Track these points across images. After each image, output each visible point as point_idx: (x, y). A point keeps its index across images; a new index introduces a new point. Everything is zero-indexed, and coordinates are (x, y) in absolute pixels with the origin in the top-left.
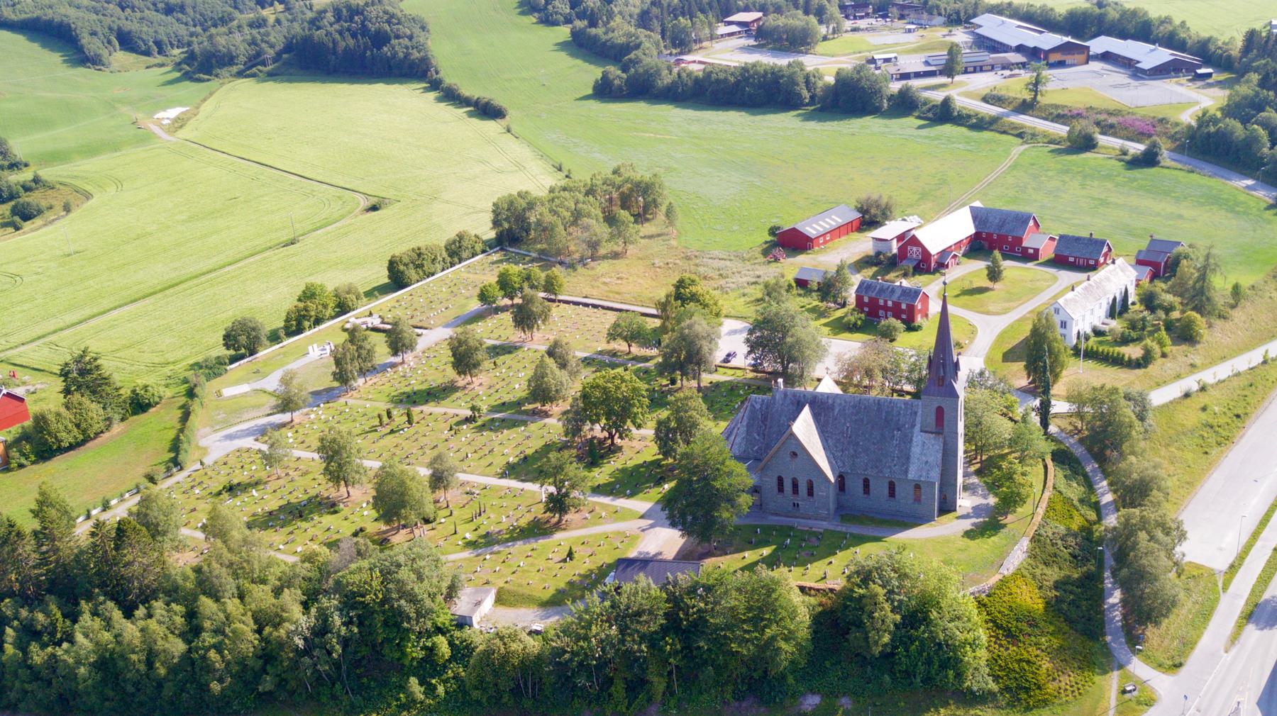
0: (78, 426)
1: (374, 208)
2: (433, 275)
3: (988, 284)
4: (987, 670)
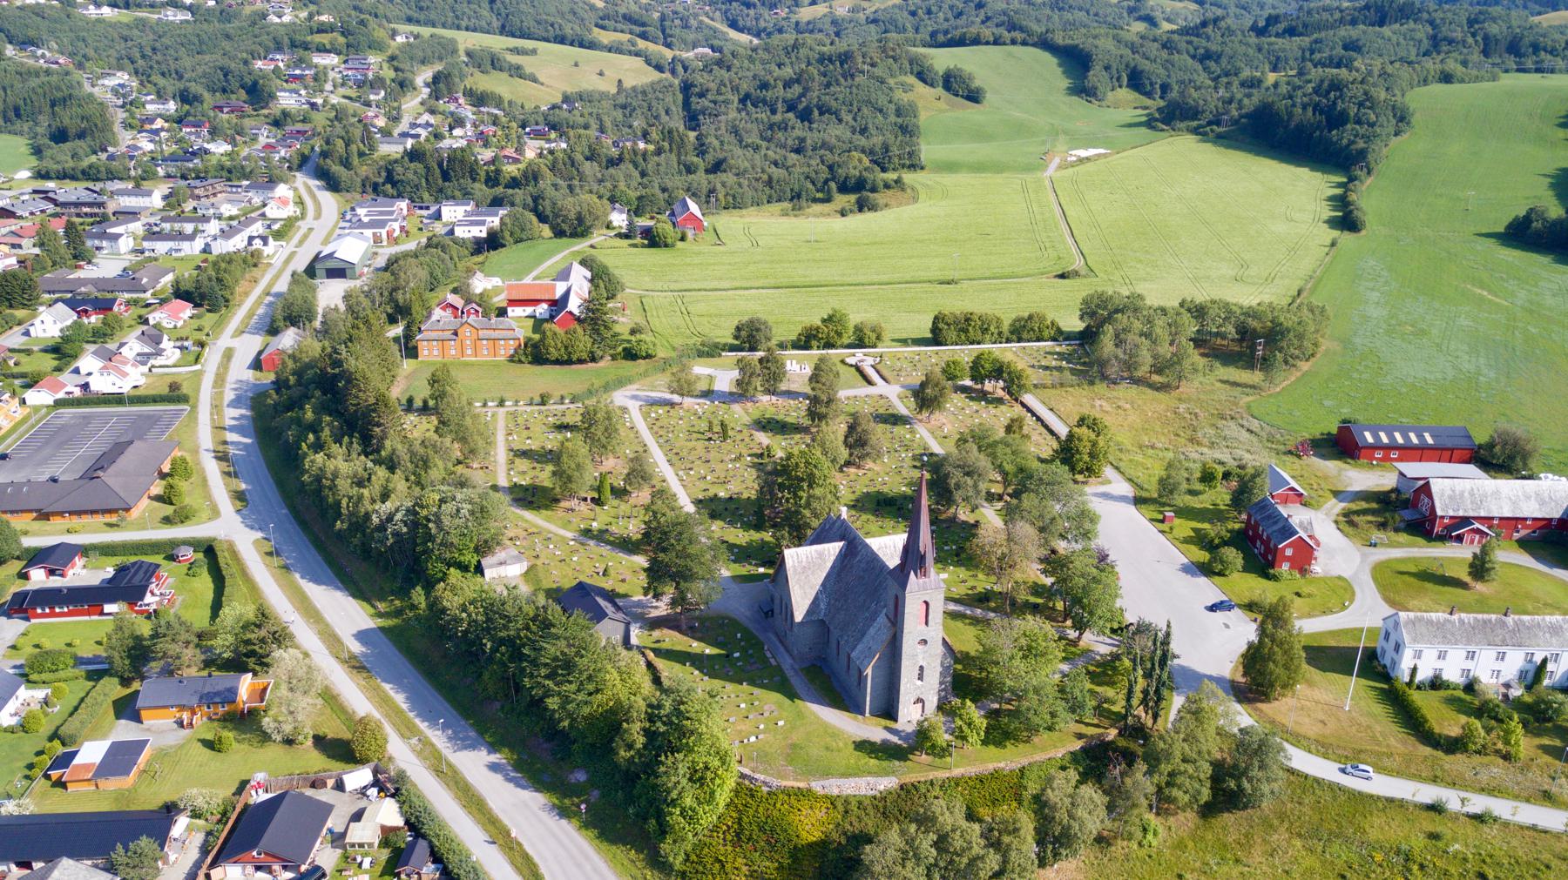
0: (566, 348)
1: (1062, 276)
2: (979, 343)
3: (1467, 579)
4: (689, 848)
